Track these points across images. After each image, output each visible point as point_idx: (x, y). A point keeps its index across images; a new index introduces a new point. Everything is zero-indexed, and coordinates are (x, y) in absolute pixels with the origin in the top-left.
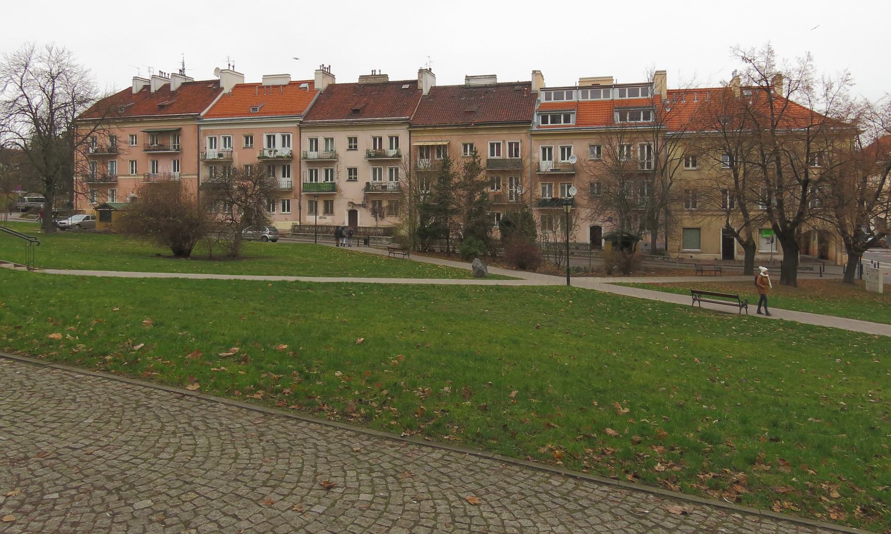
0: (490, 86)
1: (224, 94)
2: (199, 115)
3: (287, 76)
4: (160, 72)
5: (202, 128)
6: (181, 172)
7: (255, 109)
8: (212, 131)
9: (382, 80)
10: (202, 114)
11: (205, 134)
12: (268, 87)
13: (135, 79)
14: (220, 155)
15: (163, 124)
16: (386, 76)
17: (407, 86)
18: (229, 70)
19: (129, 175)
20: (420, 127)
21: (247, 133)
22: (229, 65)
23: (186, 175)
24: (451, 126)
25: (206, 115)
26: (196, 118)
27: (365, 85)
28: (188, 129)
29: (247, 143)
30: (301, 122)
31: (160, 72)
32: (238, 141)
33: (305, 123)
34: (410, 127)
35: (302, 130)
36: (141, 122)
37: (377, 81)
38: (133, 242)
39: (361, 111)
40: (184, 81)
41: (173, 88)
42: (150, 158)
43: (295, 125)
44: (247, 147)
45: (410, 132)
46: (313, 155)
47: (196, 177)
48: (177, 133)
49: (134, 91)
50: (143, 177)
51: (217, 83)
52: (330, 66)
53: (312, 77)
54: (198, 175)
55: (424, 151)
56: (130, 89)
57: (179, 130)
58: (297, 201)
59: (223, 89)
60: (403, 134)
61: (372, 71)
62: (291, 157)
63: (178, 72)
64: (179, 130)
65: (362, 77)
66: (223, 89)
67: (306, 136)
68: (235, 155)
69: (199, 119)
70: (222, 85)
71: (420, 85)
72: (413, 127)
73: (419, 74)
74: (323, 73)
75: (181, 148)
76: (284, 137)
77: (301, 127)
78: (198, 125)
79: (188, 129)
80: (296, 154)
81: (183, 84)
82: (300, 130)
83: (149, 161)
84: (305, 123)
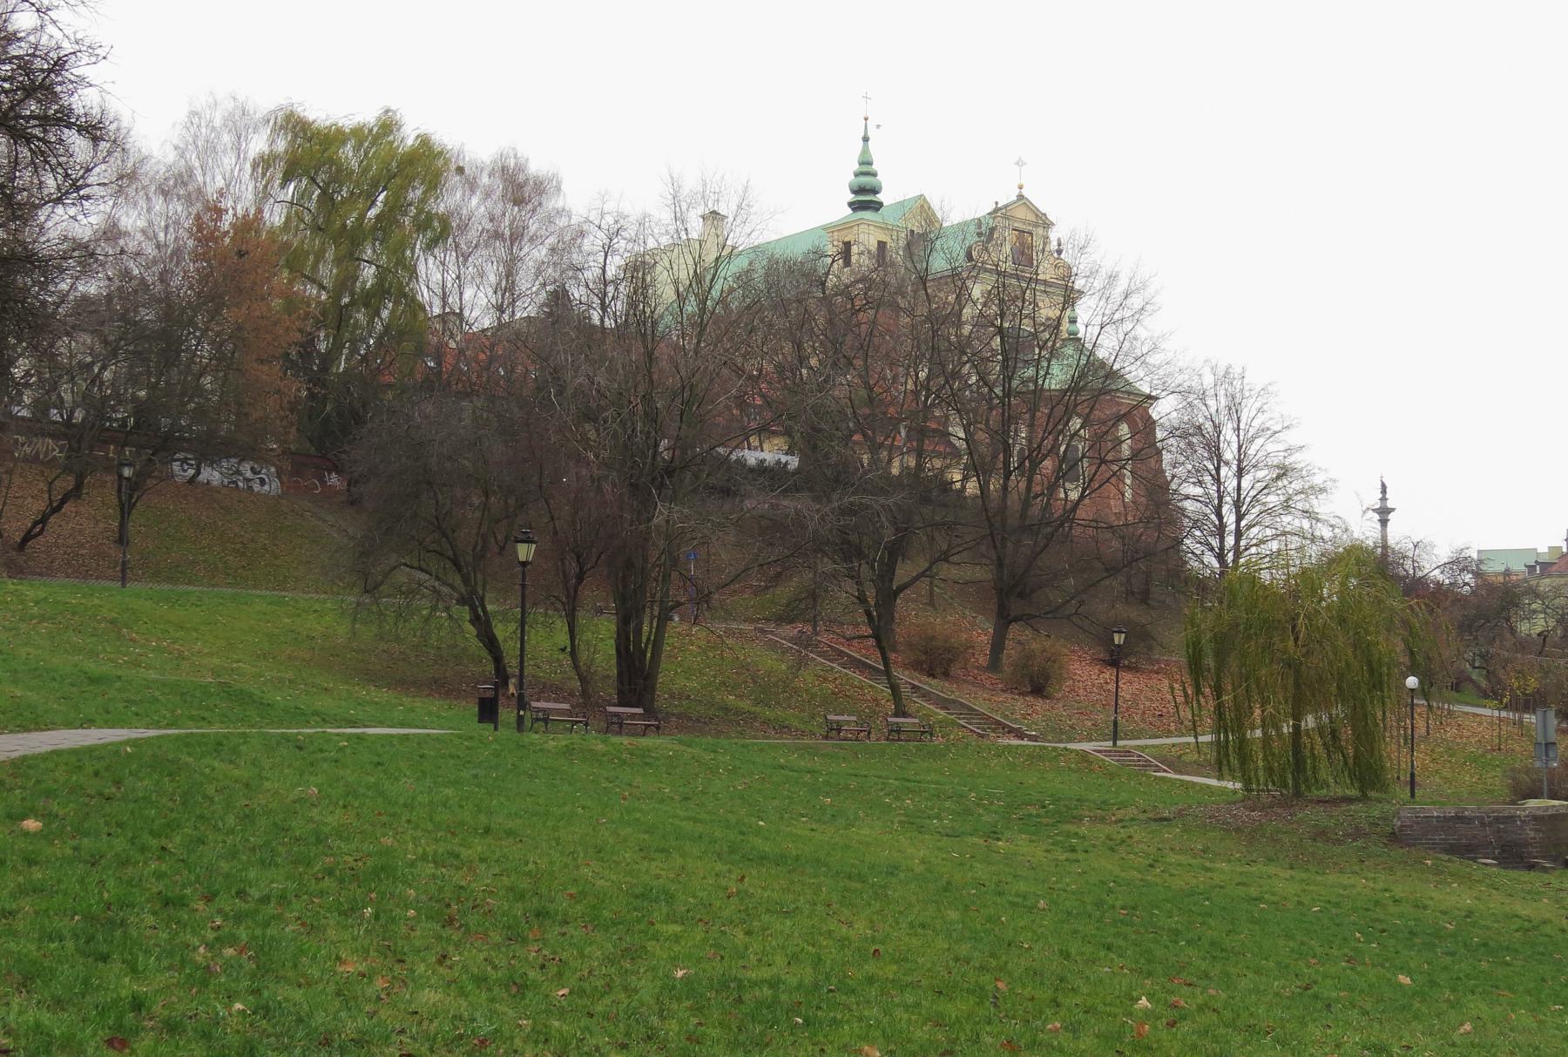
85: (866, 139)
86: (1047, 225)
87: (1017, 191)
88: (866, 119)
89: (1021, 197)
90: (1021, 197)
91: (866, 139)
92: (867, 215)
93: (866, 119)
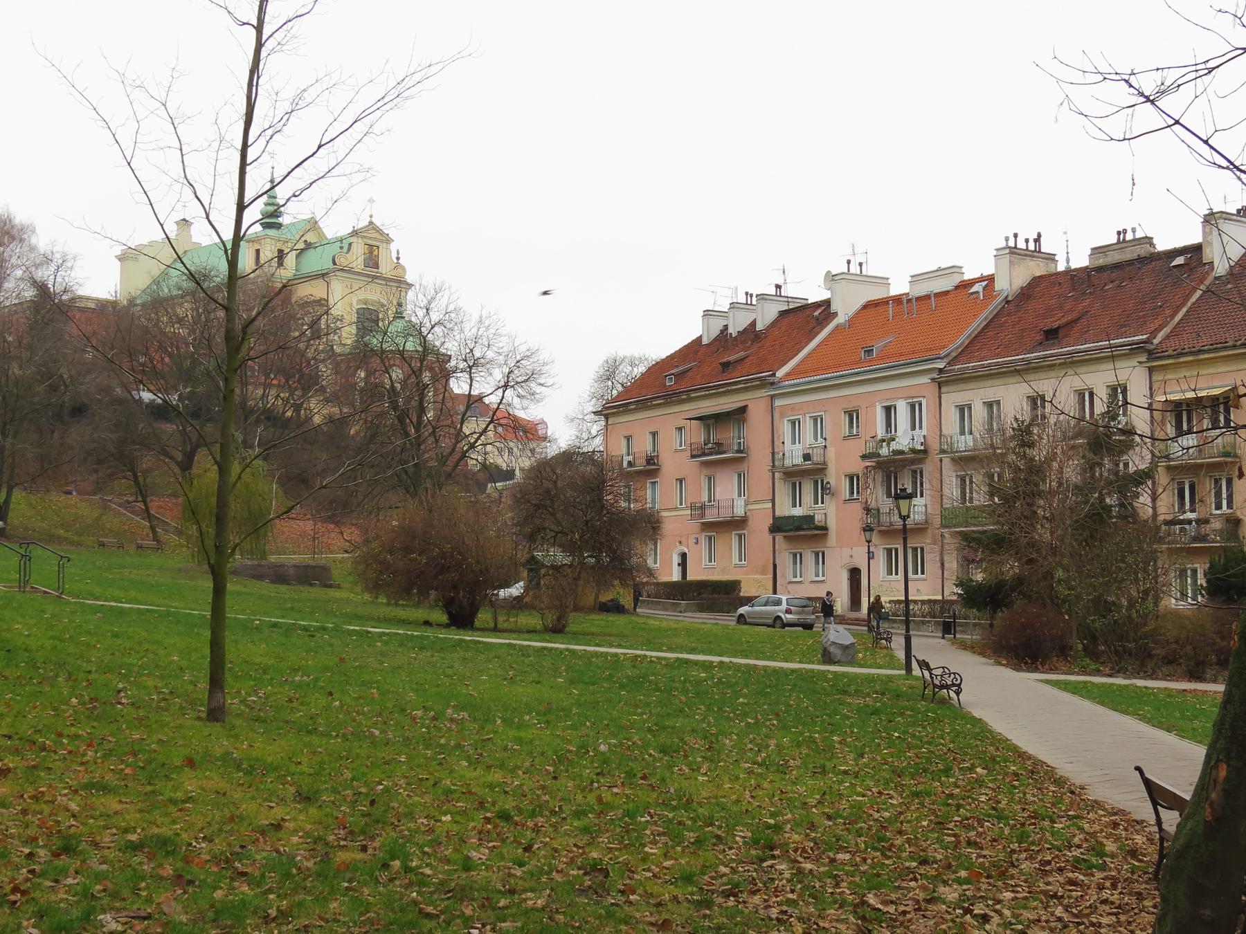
0: (1140, 259)
1: (837, 327)
2: (774, 375)
3: (956, 269)
4: (747, 294)
5: (778, 403)
6: (748, 497)
7: (869, 352)
8: (792, 408)
9: (1143, 251)
10: (780, 374)
11: (782, 416)
12: (922, 299)
13: (707, 314)
14: (807, 457)
15: (722, 400)
16: (1148, 240)
17: (1180, 260)
18: (848, 273)
19: (676, 509)
20: (1169, 357)
21: (850, 407)
22: (849, 262)
23: (756, 502)
24: (1234, 347)
25: (789, 375)
26: (764, 384)
27: (1100, 269)
28: (756, 403)
29: (851, 426)
30: (941, 371)
31: (747, 294)
32: (836, 424)
33: (947, 372)
34: (1149, 360)
35: (943, 389)
36: (689, 400)
37: (1129, 254)
38: (955, 565)
39: (1061, 334)
40: (786, 308)
41: (759, 327)
42: (705, 471)
43: (925, 380)
44: (851, 436)
45: (1151, 370)
46: (964, 443)
47: (770, 505)
48: (740, 414)
49: (705, 341)
50: (689, 512)
51: (827, 303)
52: (1039, 235)
53: (989, 270)
54: (773, 501)
55: (1181, 411)
56: (699, 339)
57: (743, 410)
58: (937, 548)
59: (835, 314)
60: (1134, 376)
61: (1119, 233)
62: (920, 455)
63: (772, 291)
64: (743, 410)
65: (1096, 251)
66: (835, 314)
67: (953, 398)
68: (831, 454)
69: (773, 384)
70: (834, 308)
71: (1207, 255)
72: (1153, 356)
73: (1204, 227)
74: (1011, 253)
75: (748, 447)
76: (913, 406)
77: (943, 381)
78: (772, 397)
79: (756, 403)
80: (934, 445)
81: (783, 314)
82: (940, 388)
83: (702, 477)
84: (947, 372)
85: (1068, 253)
86: (388, 240)
87: (369, 219)
88: (273, 168)
89: (371, 223)
90: (371, 223)
91: (1068, 253)
92: (271, 232)
93: (273, 168)
